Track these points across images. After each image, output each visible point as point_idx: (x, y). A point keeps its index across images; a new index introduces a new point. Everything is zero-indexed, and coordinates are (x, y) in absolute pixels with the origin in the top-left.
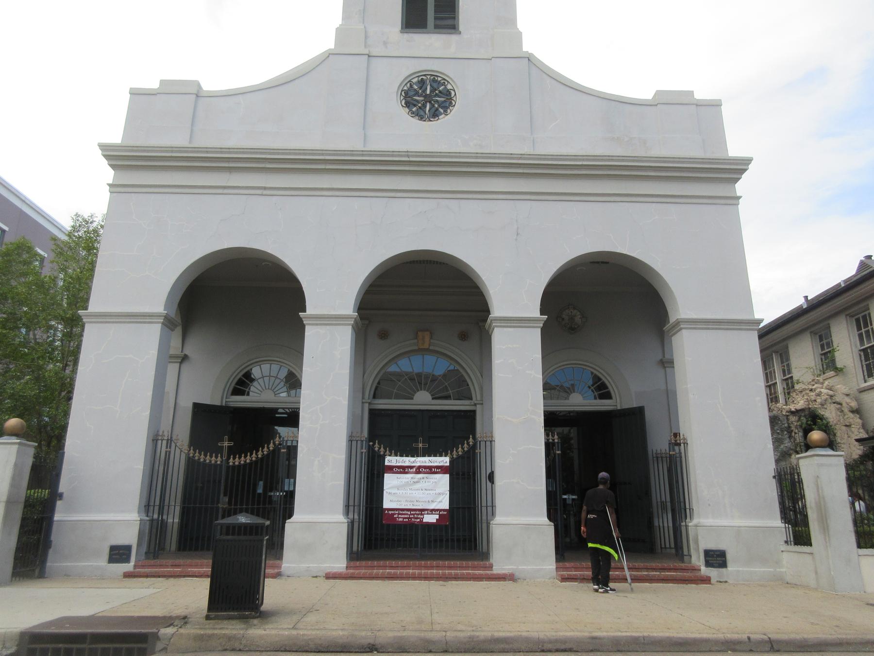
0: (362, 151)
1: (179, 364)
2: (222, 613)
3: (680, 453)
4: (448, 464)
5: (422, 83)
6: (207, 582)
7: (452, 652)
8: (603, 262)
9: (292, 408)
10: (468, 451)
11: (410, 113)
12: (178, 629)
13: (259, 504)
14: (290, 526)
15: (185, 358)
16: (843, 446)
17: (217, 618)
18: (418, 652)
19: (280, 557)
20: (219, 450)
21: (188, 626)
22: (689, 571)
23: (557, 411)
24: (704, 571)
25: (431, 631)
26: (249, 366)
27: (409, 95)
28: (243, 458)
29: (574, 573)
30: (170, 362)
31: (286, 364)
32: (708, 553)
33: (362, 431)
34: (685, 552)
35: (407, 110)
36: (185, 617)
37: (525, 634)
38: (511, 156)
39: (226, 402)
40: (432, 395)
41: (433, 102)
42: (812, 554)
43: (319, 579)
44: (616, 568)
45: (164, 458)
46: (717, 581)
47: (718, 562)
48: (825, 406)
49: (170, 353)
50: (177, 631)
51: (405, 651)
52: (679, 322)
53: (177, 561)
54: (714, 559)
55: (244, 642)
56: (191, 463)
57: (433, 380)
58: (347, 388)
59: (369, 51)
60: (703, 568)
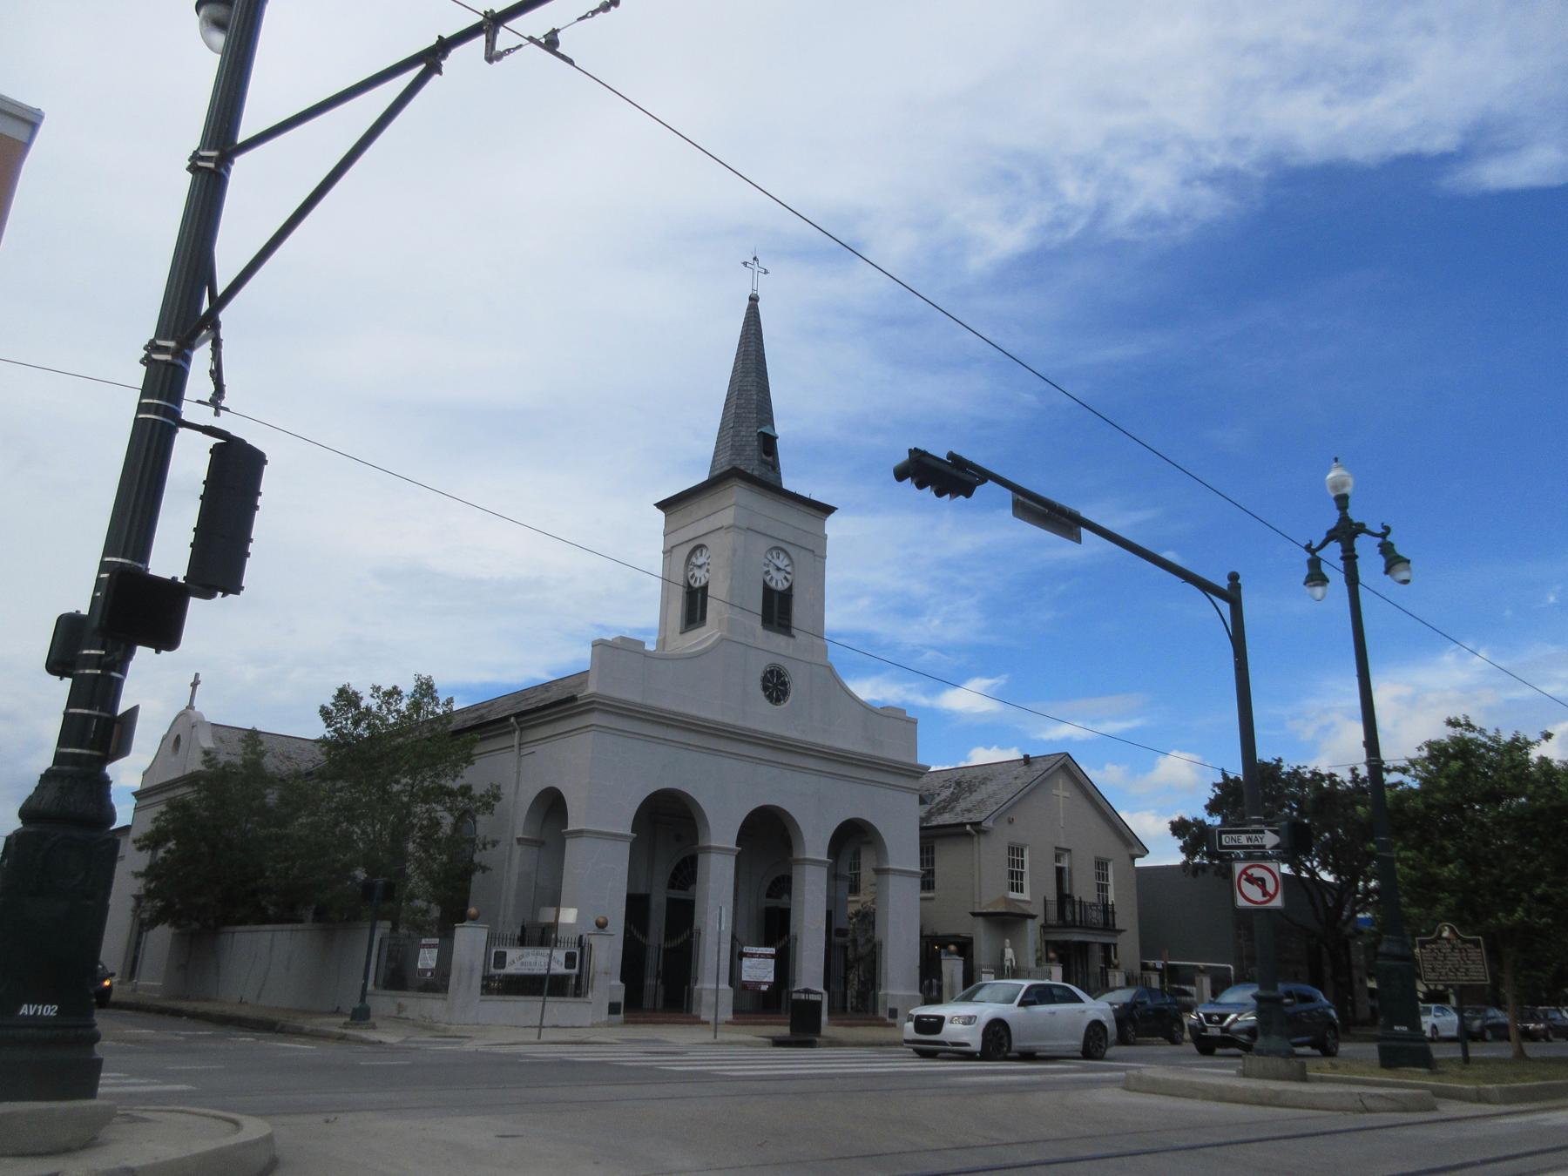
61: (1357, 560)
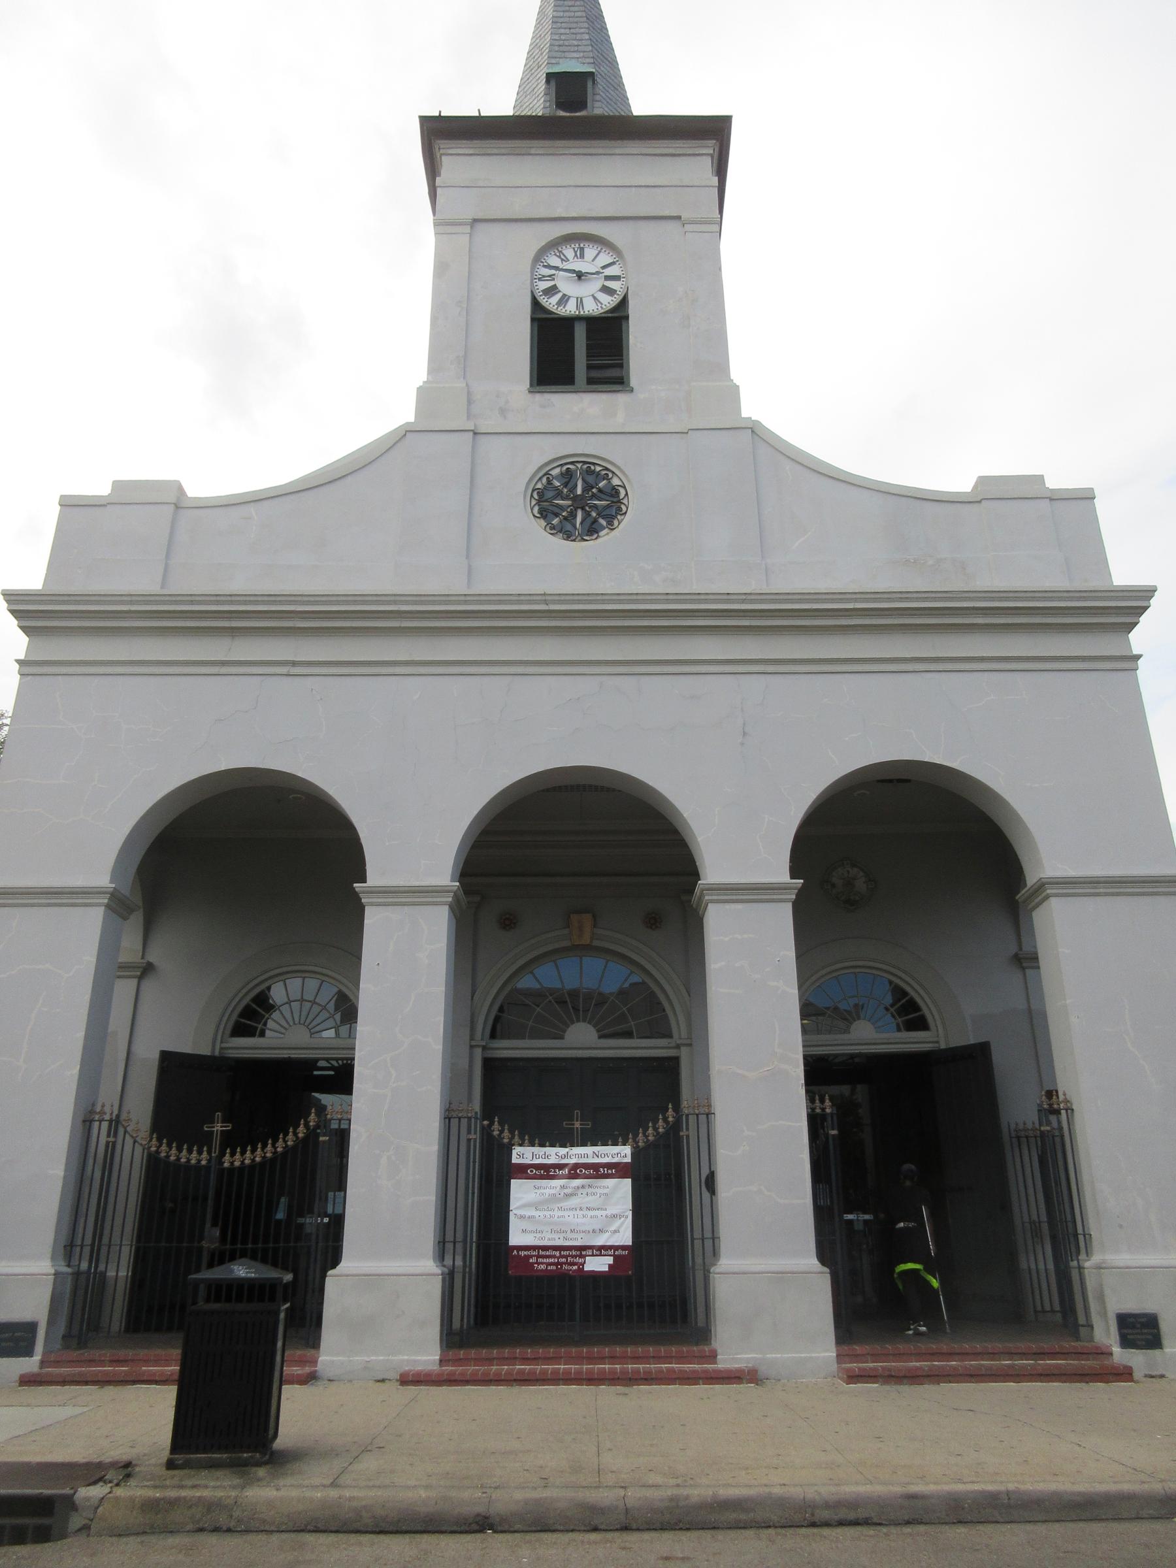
0: (465, 595)
1: (135, 981)
2: (198, 1455)
3: (1061, 1128)
4: (628, 1160)
5: (568, 476)
6: (169, 1394)
7: (638, 1529)
8: (900, 781)
9: (342, 1059)
10: (667, 1133)
11: (548, 528)
12: (111, 1487)
13: (255, 1242)
14: (335, 1285)
15: (147, 970)
17: (186, 1465)
18: (572, 1531)
19: (313, 1340)
20: (204, 1140)
21: (132, 1482)
22: (1091, 1357)
23: (829, 1055)
24: (1120, 1355)
25: (596, 1487)
26: (266, 980)
27: (545, 498)
28: (248, 1154)
29: (871, 1365)
30: (119, 977)
31: (327, 976)
32: (1125, 1321)
33: (470, 1100)
34: (1082, 1320)
35: (543, 523)
36: (128, 1464)
37: (777, 1491)
38: (728, 597)
39: (221, 1048)
40: (598, 1031)
41: (587, 508)
43: (387, 1384)
44: (951, 1354)
45: (102, 1158)
46: (1146, 1376)
47: (1144, 1337)
49: (120, 960)
50: (110, 1493)
51: (547, 1529)
52: (1043, 885)
53: (122, 1353)
54: (1136, 1331)
55: (237, 1513)
56: (154, 1166)
57: (599, 1004)
58: (441, 1019)
59: (475, 425)
60: (1116, 1350)
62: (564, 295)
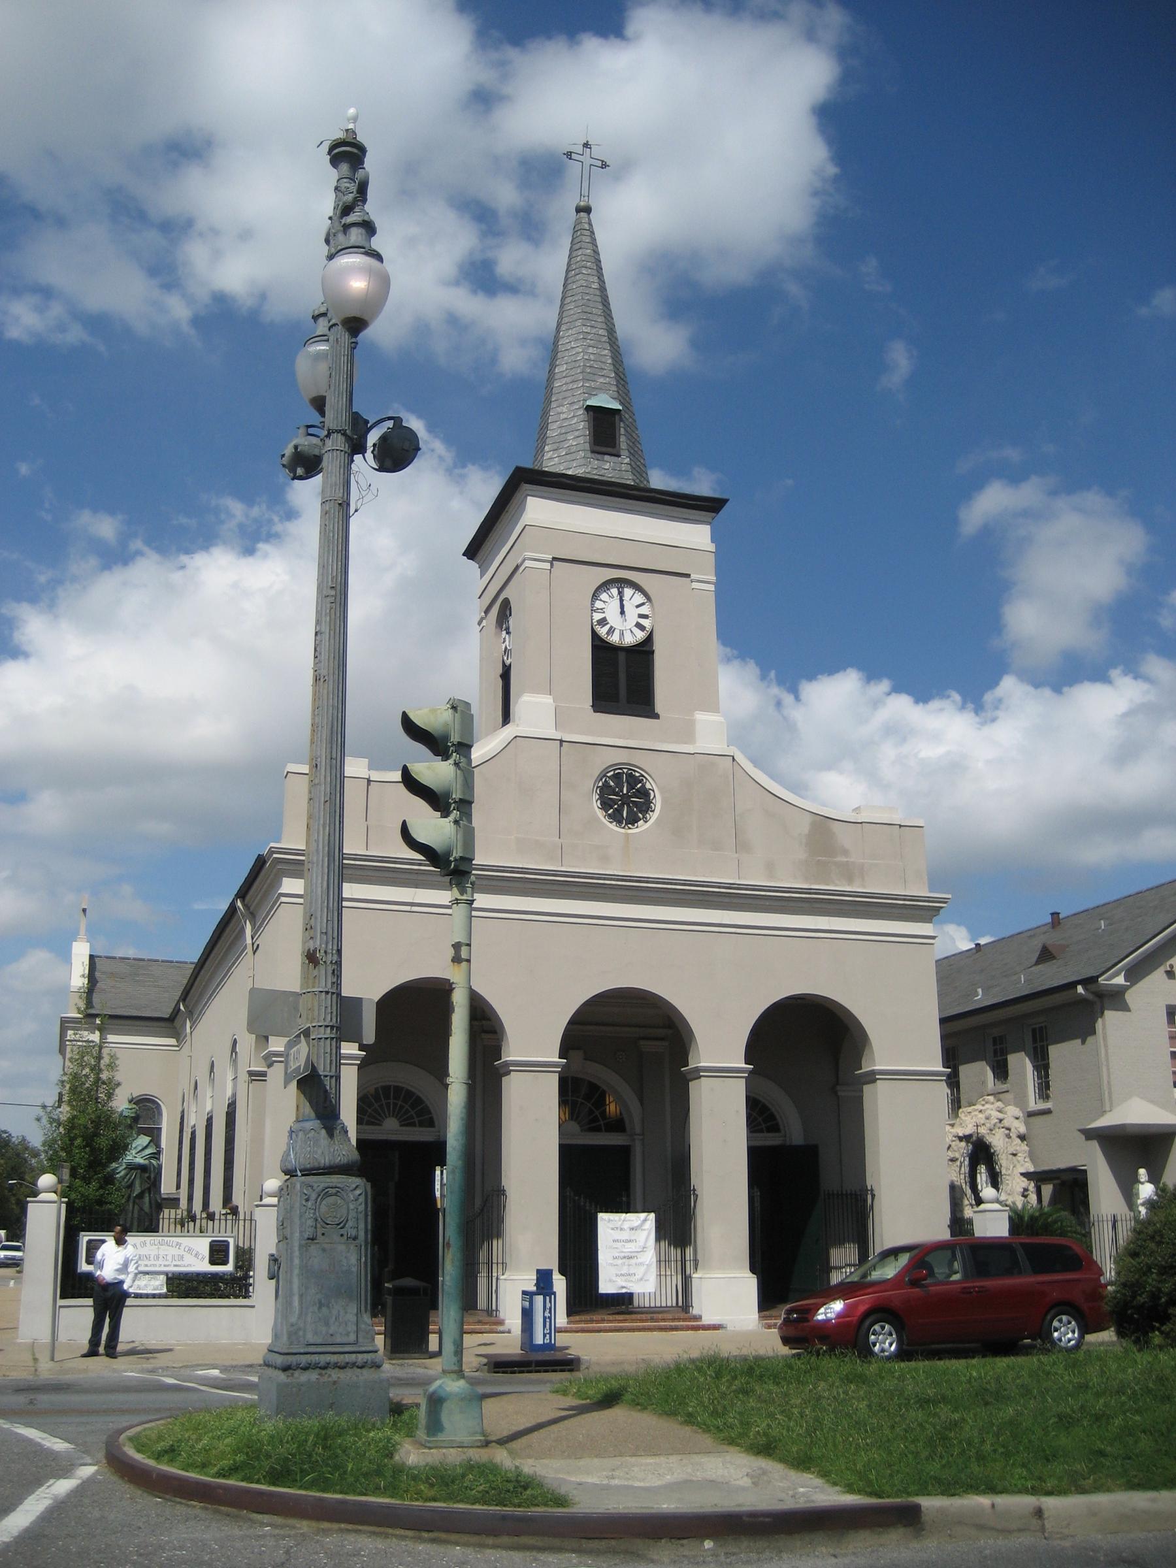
16: (1007, 1177)
42: (260, 862)
48: (993, 1132)
61: (473, 805)
62: (611, 627)
